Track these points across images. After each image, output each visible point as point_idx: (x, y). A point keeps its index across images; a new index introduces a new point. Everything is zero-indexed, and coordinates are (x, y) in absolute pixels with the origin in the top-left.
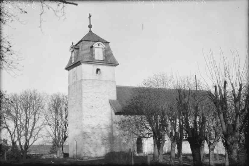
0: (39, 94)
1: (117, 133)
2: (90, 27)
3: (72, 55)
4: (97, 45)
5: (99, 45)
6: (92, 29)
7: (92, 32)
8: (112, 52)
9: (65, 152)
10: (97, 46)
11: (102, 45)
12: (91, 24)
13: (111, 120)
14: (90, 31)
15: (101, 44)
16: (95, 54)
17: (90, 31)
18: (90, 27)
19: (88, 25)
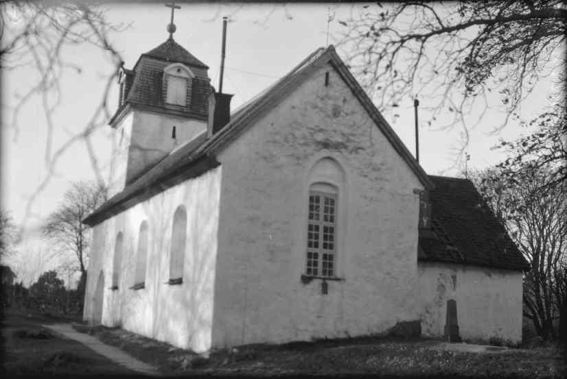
0: (75, 186)
1: (531, 346)
2: (172, 29)
3: (312, 167)
4: (176, 69)
5: (179, 70)
6: (174, 34)
7: (175, 41)
8: (210, 80)
9: (206, 345)
10: (174, 72)
11: (188, 73)
12: (175, 23)
13: (326, 337)
14: (171, 39)
15: (184, 69)
16: (166, 94)
17: (171, 39)
18: (172, 29)
19: (176, 32)
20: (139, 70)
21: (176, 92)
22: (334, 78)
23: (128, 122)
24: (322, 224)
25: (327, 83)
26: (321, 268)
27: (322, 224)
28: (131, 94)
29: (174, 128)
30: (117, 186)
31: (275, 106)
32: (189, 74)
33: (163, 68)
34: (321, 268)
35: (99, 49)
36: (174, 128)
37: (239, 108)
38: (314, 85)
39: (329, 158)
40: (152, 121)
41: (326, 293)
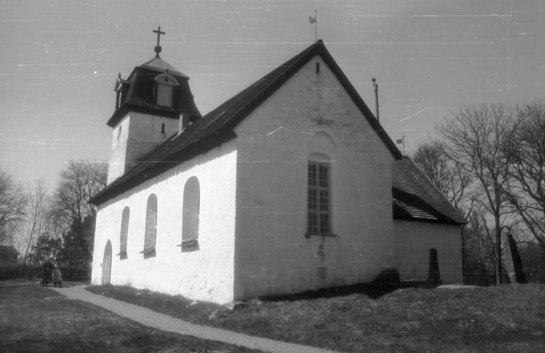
2: (158, 49)
12: (160, 45)
18: (158, 49)
20: (133, 79)
21: (164, 98)
22: (323, 67)
23: (126, 122)
24: (319, 212)
25: (318, 71)
26: (319, 224)
27: (319, 212)
28: (128, 98)
29: (163, 125)
30: (116, 170)
31: (178, 302)
32: (175, 83)
33: (153, 77)
34: (319, 224)
35: (148, 60)
36: (163, 125)
37: (156, 182)
38: (305, 75)
39: (327, 135)
40: (147, 120)
41: (312, 168)
